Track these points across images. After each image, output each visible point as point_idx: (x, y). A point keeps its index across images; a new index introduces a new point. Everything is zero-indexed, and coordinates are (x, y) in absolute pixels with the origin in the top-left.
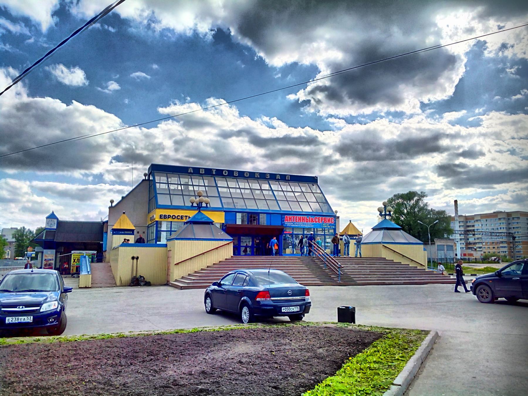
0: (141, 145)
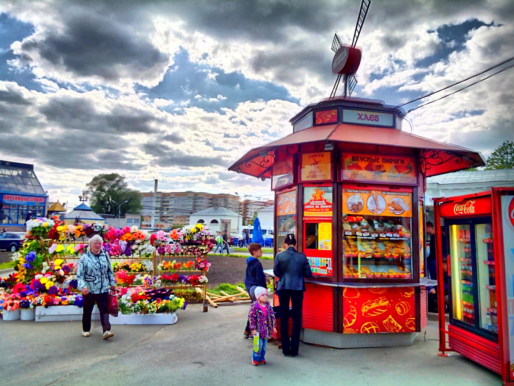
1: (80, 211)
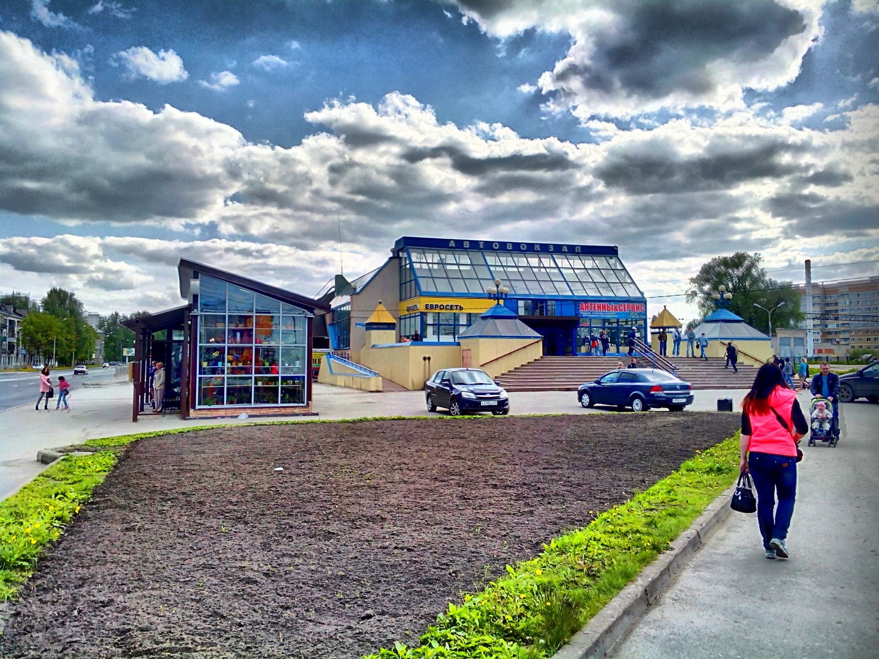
0: (274, 175)
1: (719, 324)
